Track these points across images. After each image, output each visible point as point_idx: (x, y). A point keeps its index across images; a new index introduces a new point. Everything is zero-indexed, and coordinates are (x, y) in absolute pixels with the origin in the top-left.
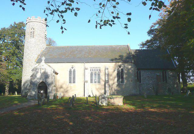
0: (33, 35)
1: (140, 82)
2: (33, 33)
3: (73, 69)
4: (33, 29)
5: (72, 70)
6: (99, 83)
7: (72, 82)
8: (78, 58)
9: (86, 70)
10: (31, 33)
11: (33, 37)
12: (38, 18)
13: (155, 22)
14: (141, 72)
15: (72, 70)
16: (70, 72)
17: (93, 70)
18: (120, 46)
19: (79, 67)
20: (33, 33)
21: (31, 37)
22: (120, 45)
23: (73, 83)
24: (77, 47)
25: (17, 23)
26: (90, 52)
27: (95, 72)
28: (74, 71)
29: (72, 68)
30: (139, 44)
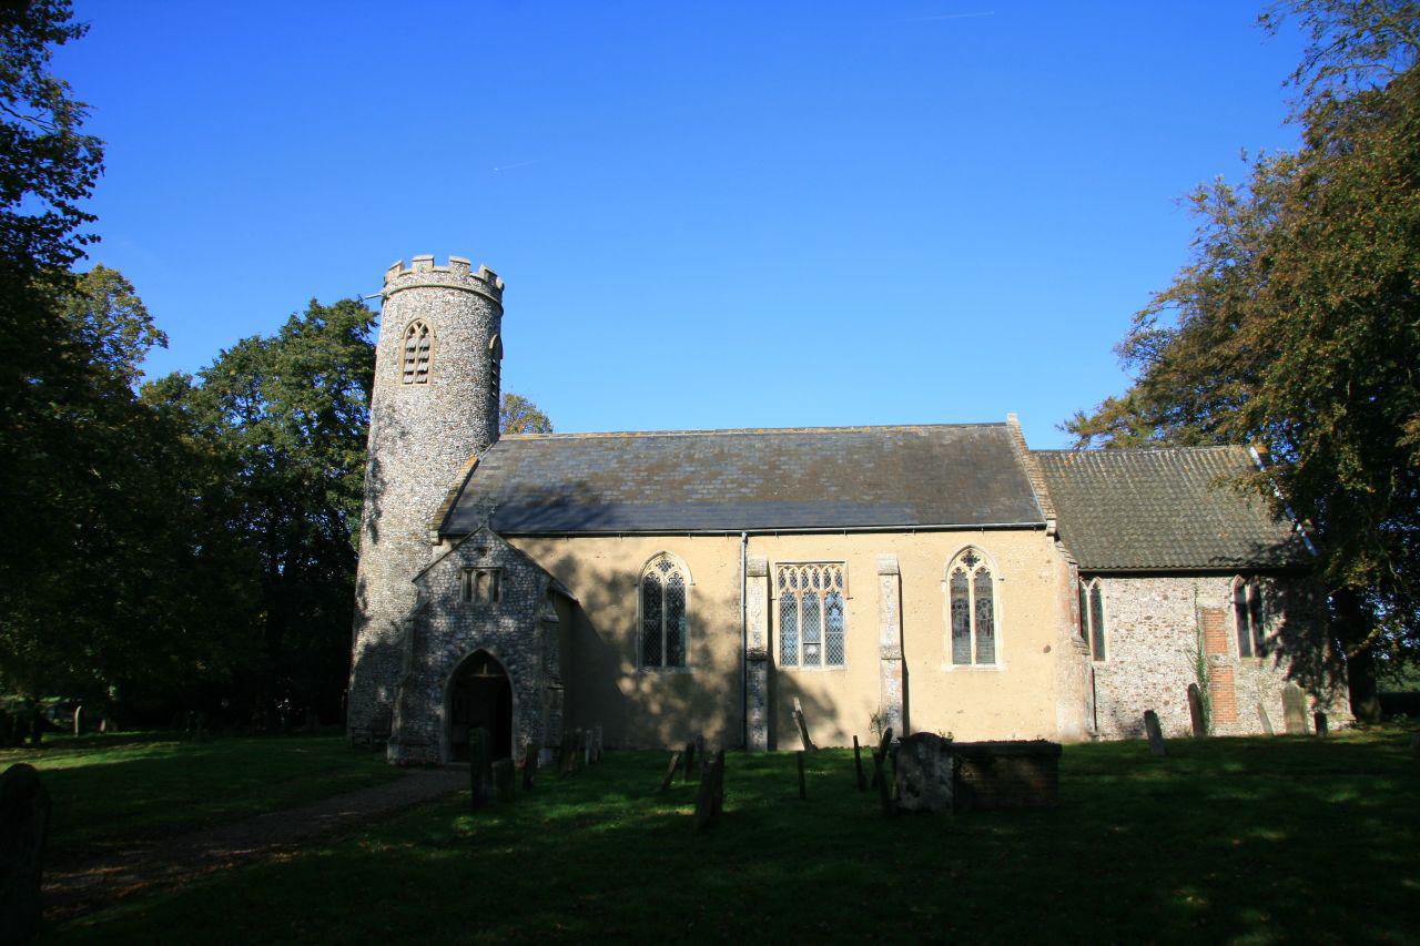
0: (423, 366)
1: (1099, 655)
2: (424, 354)
3: (976, 566)
4: (419, 332)
5: (971, 575)
6: (835, 667)
7: (664, 662)
8: (701, 503)
9: (749, 580)
10: (410, 356)
11: (422, 378)
12: (450, 267)
13: (1165, 286)
14: (1103, 594)
15: (971, 575)
16: (958, 588)
17: (794, 581)
18: (963, 427)
19: (864, 559)
20: (424, 354)
21: (409, 378)
22: (961, 421)
23: (980, 659)
24: (693, 440)
25: (327, 302)
26: (774, 467)
27: (812, 596)
28: (984, 587)
29: (970, 560)
30: (1061, 424)
